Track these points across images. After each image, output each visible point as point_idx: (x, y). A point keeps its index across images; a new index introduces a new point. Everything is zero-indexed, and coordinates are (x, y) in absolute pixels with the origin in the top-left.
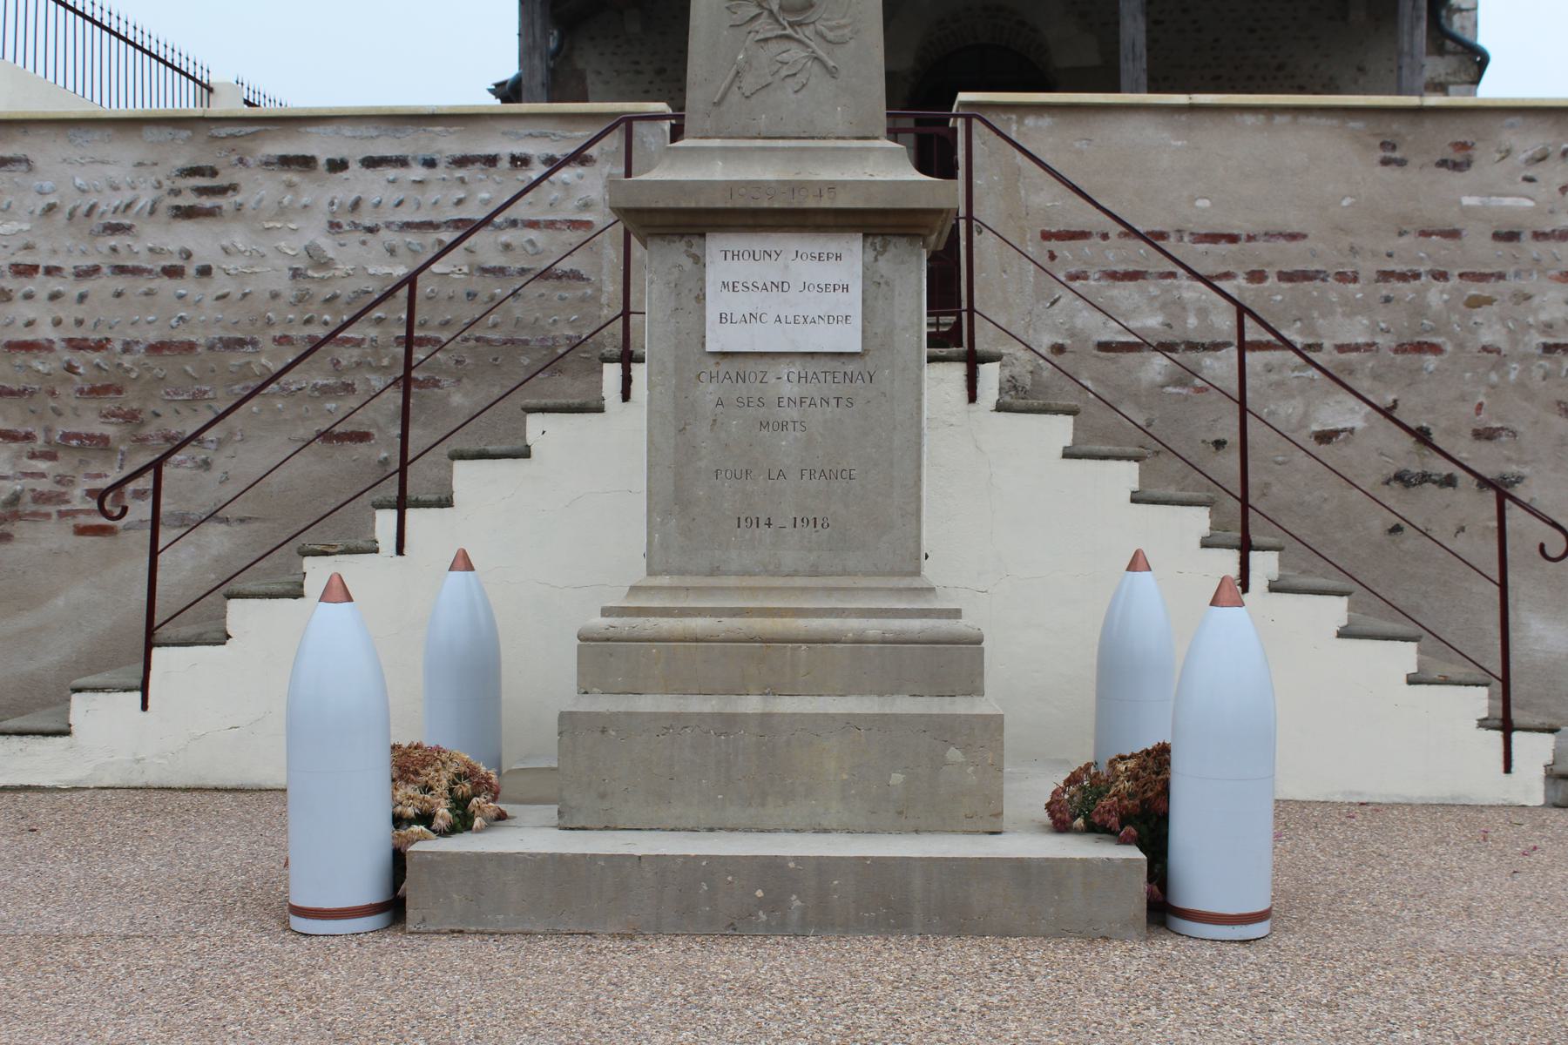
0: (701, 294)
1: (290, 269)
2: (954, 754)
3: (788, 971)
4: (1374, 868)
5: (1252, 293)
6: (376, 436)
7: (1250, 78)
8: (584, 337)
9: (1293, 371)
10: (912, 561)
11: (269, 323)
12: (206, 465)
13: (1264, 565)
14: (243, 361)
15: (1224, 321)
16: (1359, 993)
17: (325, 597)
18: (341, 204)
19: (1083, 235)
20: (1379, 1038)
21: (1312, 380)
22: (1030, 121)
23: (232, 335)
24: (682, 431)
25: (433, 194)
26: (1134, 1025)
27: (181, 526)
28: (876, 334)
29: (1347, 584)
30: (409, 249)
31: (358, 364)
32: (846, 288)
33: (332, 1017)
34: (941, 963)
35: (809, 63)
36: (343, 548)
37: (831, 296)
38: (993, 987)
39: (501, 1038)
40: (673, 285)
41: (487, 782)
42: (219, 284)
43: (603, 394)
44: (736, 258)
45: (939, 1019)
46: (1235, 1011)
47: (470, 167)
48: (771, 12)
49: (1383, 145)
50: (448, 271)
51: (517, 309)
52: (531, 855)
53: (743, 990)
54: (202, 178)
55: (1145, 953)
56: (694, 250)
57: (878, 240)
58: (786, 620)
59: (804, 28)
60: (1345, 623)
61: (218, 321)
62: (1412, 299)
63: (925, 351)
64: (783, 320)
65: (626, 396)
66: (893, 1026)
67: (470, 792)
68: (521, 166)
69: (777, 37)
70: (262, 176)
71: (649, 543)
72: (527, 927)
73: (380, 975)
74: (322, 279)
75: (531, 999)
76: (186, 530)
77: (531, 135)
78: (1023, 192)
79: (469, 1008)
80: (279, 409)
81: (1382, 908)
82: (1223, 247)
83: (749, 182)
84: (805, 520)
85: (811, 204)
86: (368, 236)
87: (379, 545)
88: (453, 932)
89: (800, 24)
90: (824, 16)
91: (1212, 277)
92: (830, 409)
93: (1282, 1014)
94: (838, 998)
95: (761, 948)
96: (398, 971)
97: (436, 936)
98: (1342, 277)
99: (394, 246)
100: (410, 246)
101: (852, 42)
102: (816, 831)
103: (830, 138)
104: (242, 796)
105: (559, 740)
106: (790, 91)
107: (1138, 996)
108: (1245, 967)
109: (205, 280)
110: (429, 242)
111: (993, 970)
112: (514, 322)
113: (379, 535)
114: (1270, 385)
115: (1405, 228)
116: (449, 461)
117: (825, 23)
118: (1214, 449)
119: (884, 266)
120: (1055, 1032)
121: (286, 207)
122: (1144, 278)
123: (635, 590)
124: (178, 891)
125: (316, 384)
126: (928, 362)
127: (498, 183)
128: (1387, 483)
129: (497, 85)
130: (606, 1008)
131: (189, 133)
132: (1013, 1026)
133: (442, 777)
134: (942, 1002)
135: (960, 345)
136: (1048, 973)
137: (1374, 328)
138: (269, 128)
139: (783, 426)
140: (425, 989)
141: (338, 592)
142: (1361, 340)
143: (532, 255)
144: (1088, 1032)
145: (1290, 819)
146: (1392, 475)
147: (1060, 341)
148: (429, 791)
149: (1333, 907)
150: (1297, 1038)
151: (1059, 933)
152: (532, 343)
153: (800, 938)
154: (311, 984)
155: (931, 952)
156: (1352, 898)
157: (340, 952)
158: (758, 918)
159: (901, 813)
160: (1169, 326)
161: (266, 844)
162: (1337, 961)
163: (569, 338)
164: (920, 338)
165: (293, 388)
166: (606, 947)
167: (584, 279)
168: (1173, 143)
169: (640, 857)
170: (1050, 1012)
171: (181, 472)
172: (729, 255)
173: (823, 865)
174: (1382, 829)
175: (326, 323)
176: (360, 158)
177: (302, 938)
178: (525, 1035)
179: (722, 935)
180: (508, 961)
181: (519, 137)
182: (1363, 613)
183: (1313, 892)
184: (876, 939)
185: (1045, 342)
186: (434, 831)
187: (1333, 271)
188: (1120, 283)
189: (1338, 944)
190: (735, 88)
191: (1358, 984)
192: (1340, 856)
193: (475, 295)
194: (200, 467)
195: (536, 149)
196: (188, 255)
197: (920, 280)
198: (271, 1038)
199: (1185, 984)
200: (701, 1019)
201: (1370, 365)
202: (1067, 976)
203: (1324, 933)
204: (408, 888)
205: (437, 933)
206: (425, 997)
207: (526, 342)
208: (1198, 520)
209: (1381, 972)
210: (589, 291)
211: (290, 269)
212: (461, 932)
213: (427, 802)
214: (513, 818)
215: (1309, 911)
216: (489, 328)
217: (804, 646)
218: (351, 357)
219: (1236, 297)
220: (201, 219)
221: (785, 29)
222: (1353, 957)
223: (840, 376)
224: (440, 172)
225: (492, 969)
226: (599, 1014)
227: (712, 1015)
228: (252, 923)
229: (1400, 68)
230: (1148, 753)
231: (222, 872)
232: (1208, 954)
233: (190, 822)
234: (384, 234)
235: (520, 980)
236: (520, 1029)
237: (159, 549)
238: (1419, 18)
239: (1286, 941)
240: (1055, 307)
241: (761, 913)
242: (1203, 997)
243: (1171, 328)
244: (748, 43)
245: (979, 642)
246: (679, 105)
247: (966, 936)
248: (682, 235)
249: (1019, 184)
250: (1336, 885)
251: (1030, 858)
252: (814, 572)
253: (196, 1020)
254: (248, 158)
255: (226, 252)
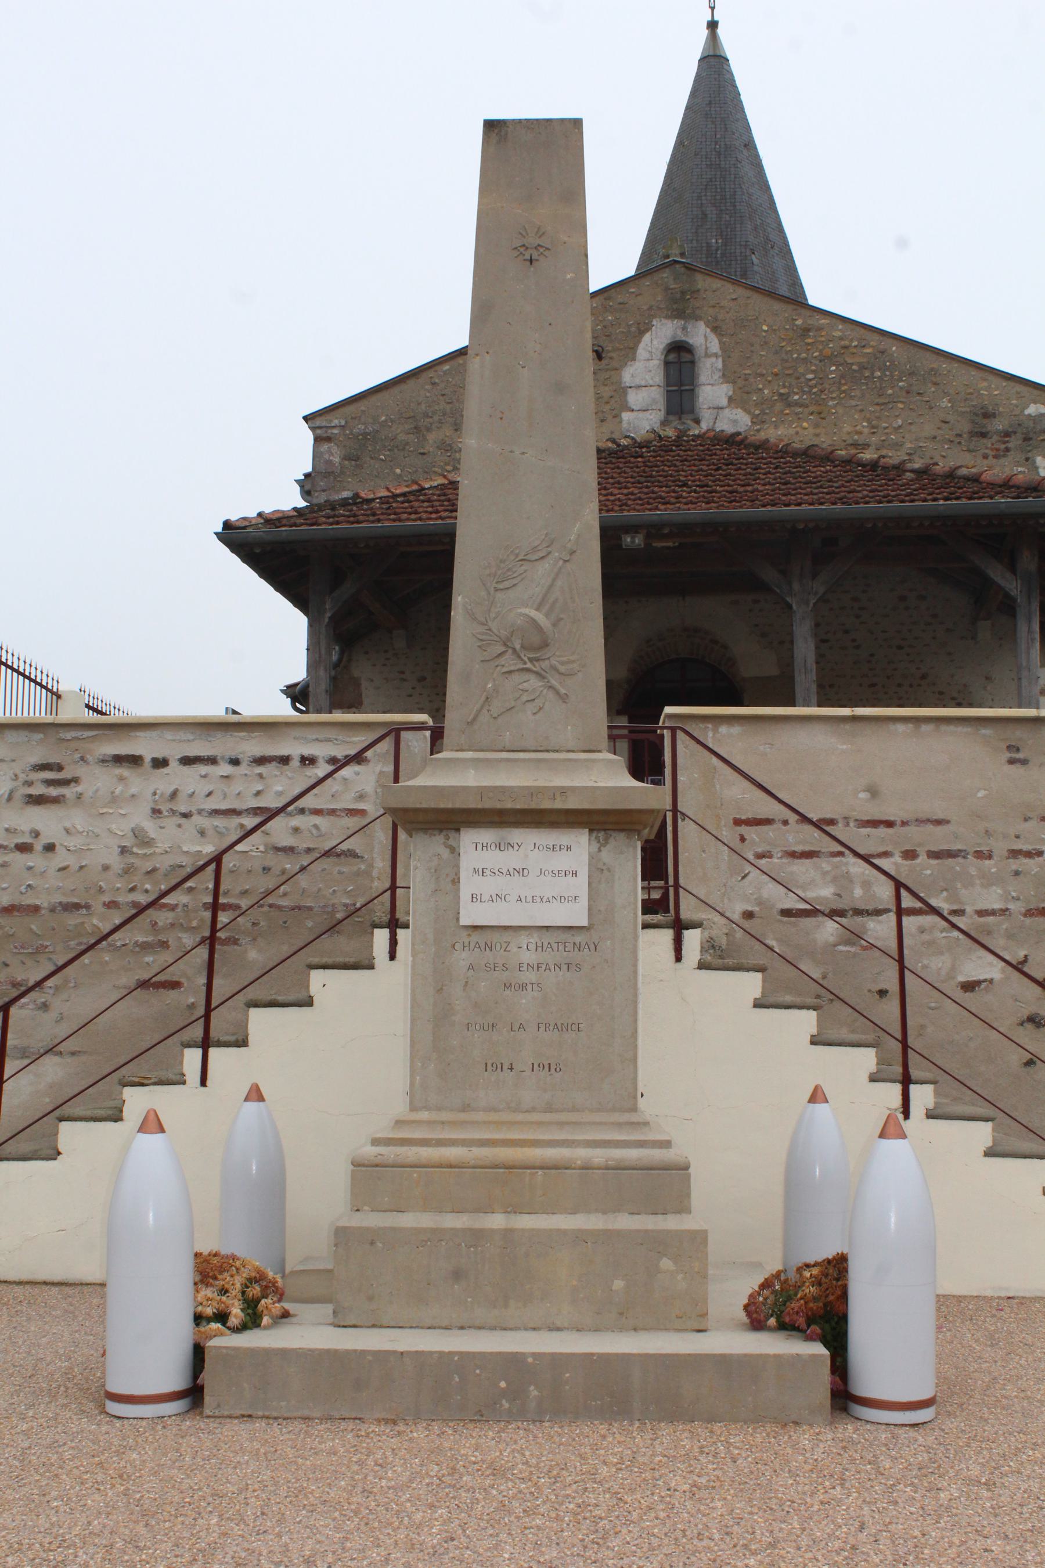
0: (456, 878)
1: (119, 847)
2: (666, 1264)
3: (527, 1453)
4: (1021, 1356)
5: (906, 868)
6: (185, 985)
7: (900, 698)
8: (358, 905)
9: (942, 932)
10: (630, 1100)
11: (101, 890)
12: (45, 1007)
13: (922, 1096)
14: (79, 921)
15: (884, 892)
16: (1012, 1472)
17: (142, 1129)
18: (162, 794)
19: (768, 822)
20: (1031, 1514)
21: (958, 939)
22: (723, 729)
23: (70, 900)
24: (440, 991)
25: (237, 787)
26: (822, 1503)
27: (22, 1058)
28: (599, 911)
29: (991, 1112)
30: (217, 831)
31: (172, 925)
32: (575, 874)
33: (140, 1494)
34: (657, 1446)
35: (545, 691)
36: (156, 1080)
37: (563, 881)
38: (702, 1469)
39: (283, 1514)
40: (433, 871)
41: (274, 1286)
42: (61, 858)
43: (374, 954)
44: (485, 848)
45: (656, 1498)
46: (908, 1489)
47: (268, 765)
48: (514, 650)
49: (1009, 748)
50: (247, 850)
51: (303, 881)
52: (310, 1350)
53: (489, 1472)
54: (50, 772)
55: (830, 1437)
56: (451, 842)
57: (601, 834)
58: (526, 1150)
59: (541, 663)
60: (990, 1144)
61: (59, 888)
62: (1037, 872)
63: (640, 918)
64: (523, 900)
65: (392, 956)
66: (617, 1505)
67: (259, 1294)
68: (309, 764)
69: (518, 670)
70: (98, 770)
71: (412, 1084)
72: (306, 1413)
73: (181, 1455)
74: (145, 855)
75: (309, 1479)
76: (26, 1062)
77: (317, 739)
78: (718, 787)
79: (256, 1486)
80: (106, 961)
81: (1029, 1393)
82: (882, 831)
83: (496, 787)
84: (541, 1065)
85: (546, 805)
86: (183, 821)
87: (187, 1078)
88: (243, 1416)
89: (538, 660)
90: (557, 653)
91: (873, 856)
92: (561, 973)
93: (948, 1493)
94: (570, 1478)
95: (504, 1432)
96: (197, 1452)
97: (228, 1420)
98: (979, 855)
99: (204, 829)
100: (218, 829)
101: (580, 674)
102: (551, 1330)
103: (562, 751)
104: (67, 1290)
105: (335, 1251)
106: (529, 713)
107: (825, 1476)
108: (915, 1449)
109: (50, 855)
110: (232, 826)
111: (702, 1452)
112: (300, 892)
113: (186, 1069)
114: (923, 944)
115: (1029, 815)
116: (246, 1009)
117: (558, 659)
118: (878, 997)
119: (606, 855)
120: (755, 1510)
121: (117, 796)
122: (818, 857)
123: (399, 1123)
124: (12, 1375)
125: (137, 941)
126: (642, 928)
127: (290, 778)
128: (1022, 1024)
129: (288, 687)
130: (373, 1488)
131: (41, 736)
132: (719, 1504)
133: (236, 1281)
134: (658, 1482)
135: (667, 911)
136: (748, 1456)
137: (1006, 897)
138: (106, 732)
139: (523, 987)
140: (219, 1468)
141: (153, 1124)
142: (997, 906)
143: (317, 837)
144: (783, 1510)
145: (949, 1312)
146: (1025, 1017)
147: (750, 909)
148: (225, 1293)
149: (988, 1393)
150: (961, 1514)
151: (757, 1419)
152: (316, 909)
153: (538, 1423)
154: (123, 1463)
155: (648, 1436)
156: (1004, 1384)
157: (147, 1434)
158: (502, 1405)
159: (621, 1314)
160: (839, 895)
161: (85, 1333)
162: (993, 1442)
163: (346, 905)
164: (635, 904)
165: (119, 944)
166: (373, 1431)
167: (358, 857)
168: (840, 747)
169: (402, 1353)
170: (750, 1491)
171: (24, 1012)
172: (479, 847)
173: (557, 1361)
174: (1026, 1320)
175: (147, 891)
176: (179, 756)
177: (115, 1421)
178: (304, 1512)
179: (471, 1420)
180: (290, 1443)
181: (308, 741)
182: (1005, 1134)
183: (971, 1379)
184: (601, 1424)
185: (736, 909)
186: (229, 1328)
187: (971, 850)
188: (799, 861)
189: (993, 1427)
190: (485, 711)
191: (1011, 1464)
192: (992, 1345)
193: (269, 869)
194: (39, 1008)
195: (321, 751)
196: (37, 834)
197: (636, 867)
198: (88, 1513)
199: (865, 1465)
200: (454, 1498)
201: (1004, 927)
202: (765, 1458)
203: (981, 1417)
204: (205, 1377)
205: (230, 1417)
206: (219, 1476)
207: (310, 909)
208: (867, 1059)
209: (1030, 1453)
210: (363, 867)
211: (119, 847)
212: (250, 1416)
213: (222, 1302)
214: (295, 1316)
215: (968, 1396)
216: (281, 896)
217: (540, 1172)
218: (167, 919)
219: (893, 873)
220: (48, 805)
221: (525, 663)
222: (1006, 1438)
223: (570, 947)
224: (243, 769)
225: (276, 1451)
226: (367, 1492)
227: (463, 1494)
228: (74, 1406)
229: (1020, 679)
230: (829, 1261)
231: (49, 1359)
232: (883, 1436)
233: (22, 1312)
234: (197, 819)
235: (300, 1461)
236: (299, 1506)
237: (5, 1078)
238: (1033, 640)
239: (950, 1424)
240: (745, 880)
241: (504, 1402)
242: (880, 1477)
243: (841, 897)
244: (495, 675)
245: (686, 1168)
246: (438, 712)
247: (678, 1421)
248: (441, 830)
249: (715, 780)
250: (990, 1373)
251: (731, 1354)
252: (549, 1109)
253: (24, 1495)
254: (88, 756)
255: (68, 832)
